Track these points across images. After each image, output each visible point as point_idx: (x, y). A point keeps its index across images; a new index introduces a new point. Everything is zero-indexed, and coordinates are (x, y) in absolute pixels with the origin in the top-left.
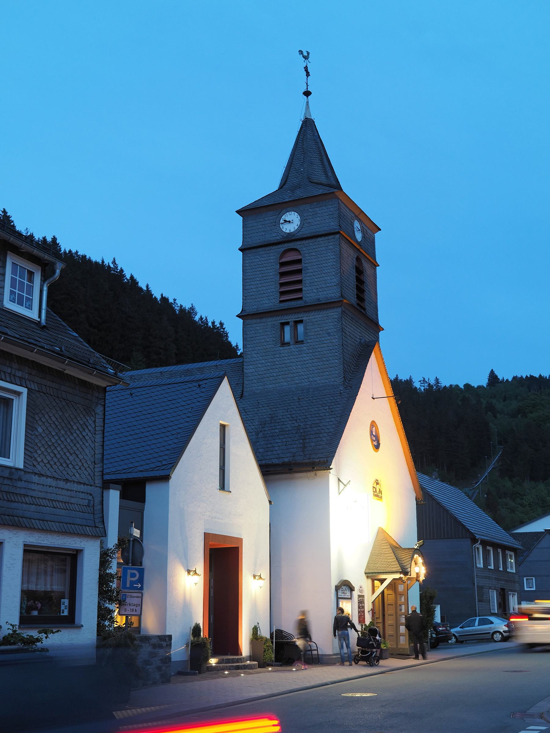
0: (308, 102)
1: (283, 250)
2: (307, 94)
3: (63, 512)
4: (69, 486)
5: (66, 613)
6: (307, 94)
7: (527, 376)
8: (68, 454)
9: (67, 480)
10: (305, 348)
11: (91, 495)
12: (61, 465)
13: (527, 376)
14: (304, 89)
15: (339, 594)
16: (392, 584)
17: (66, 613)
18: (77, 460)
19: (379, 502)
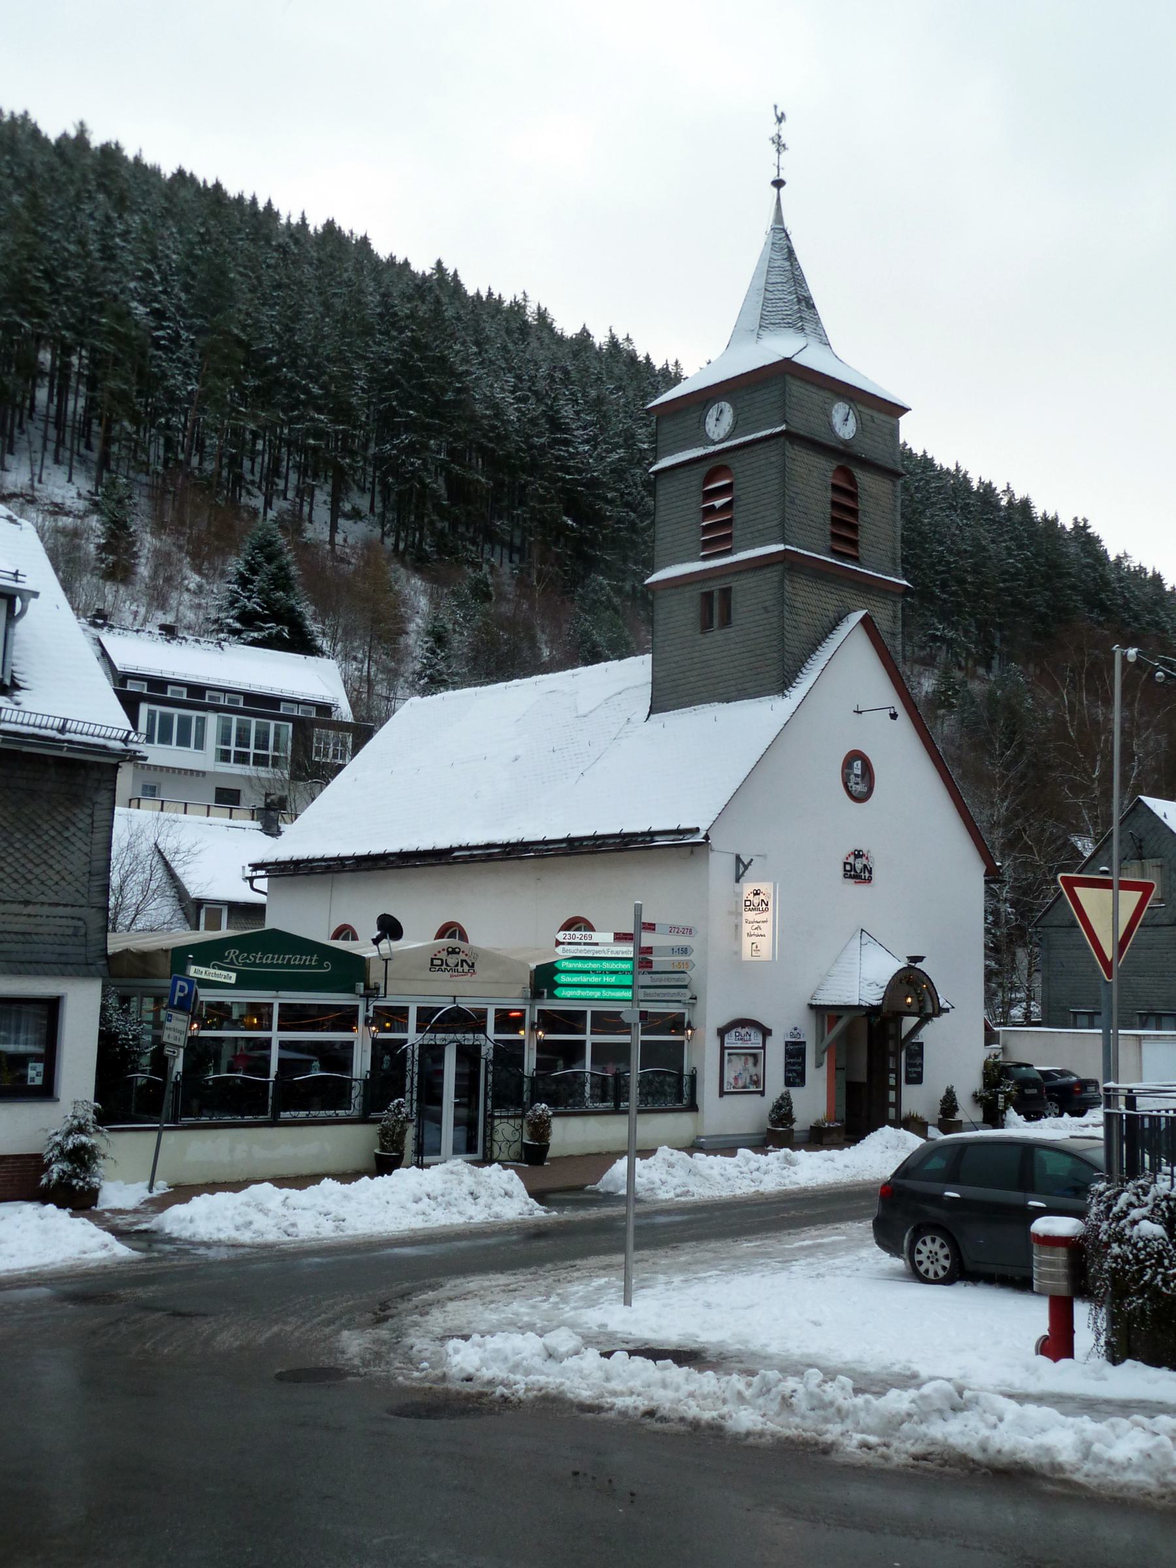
0: (779, 199)
1: (707, 468)
2: (778, 184)
3: (19, 947)
4: (30, 909)
5: (39, 1081)
6: (778, 184)
7: (657, 706)
8: (30, 866)
9: (27, 903)
10: (733, 635)
11: (79, 919)
12: (15, 881)
13: (657, 706)
14: (773, 176)
15: (726, 1040)
16: (766, 1032)
17: (39, 1081)
18: (51, 872)
19: (863, 888)
